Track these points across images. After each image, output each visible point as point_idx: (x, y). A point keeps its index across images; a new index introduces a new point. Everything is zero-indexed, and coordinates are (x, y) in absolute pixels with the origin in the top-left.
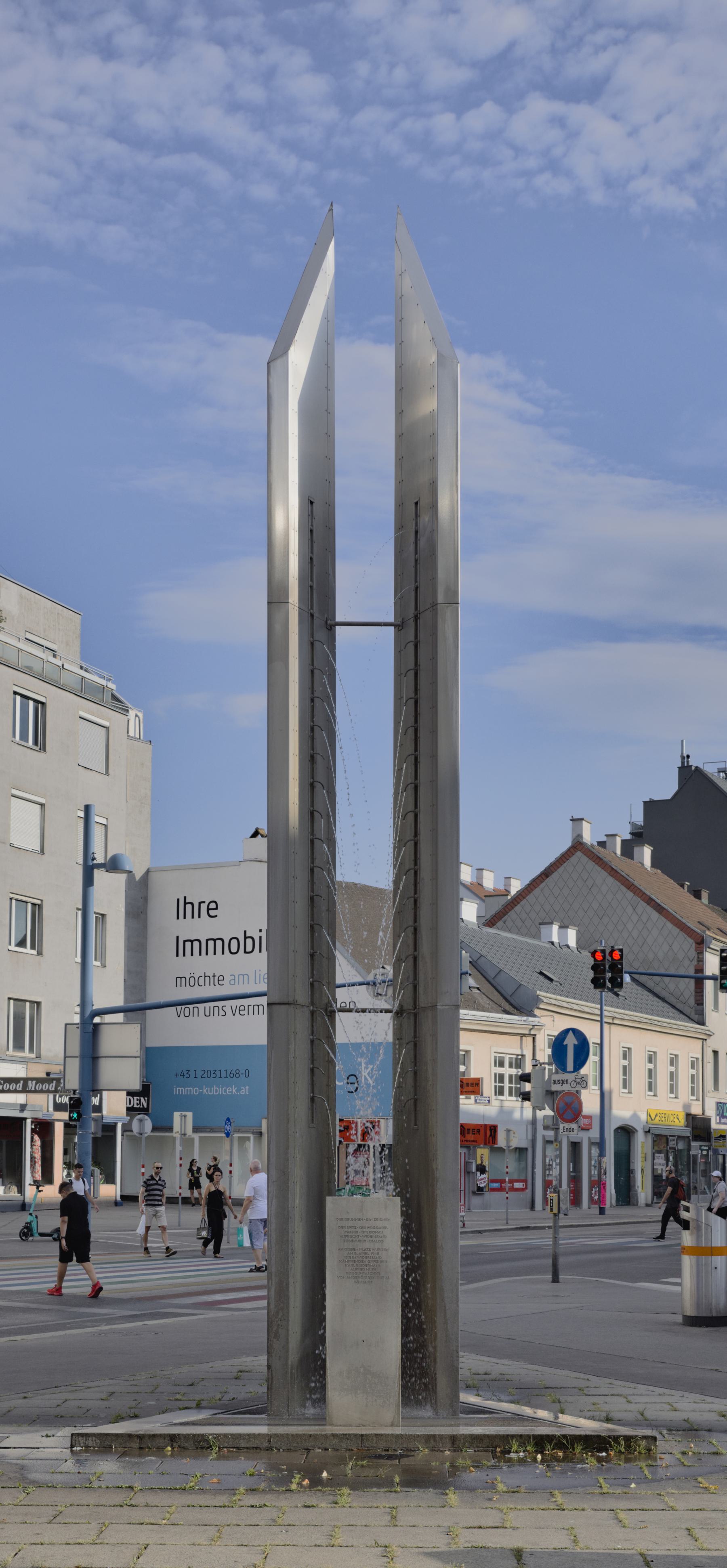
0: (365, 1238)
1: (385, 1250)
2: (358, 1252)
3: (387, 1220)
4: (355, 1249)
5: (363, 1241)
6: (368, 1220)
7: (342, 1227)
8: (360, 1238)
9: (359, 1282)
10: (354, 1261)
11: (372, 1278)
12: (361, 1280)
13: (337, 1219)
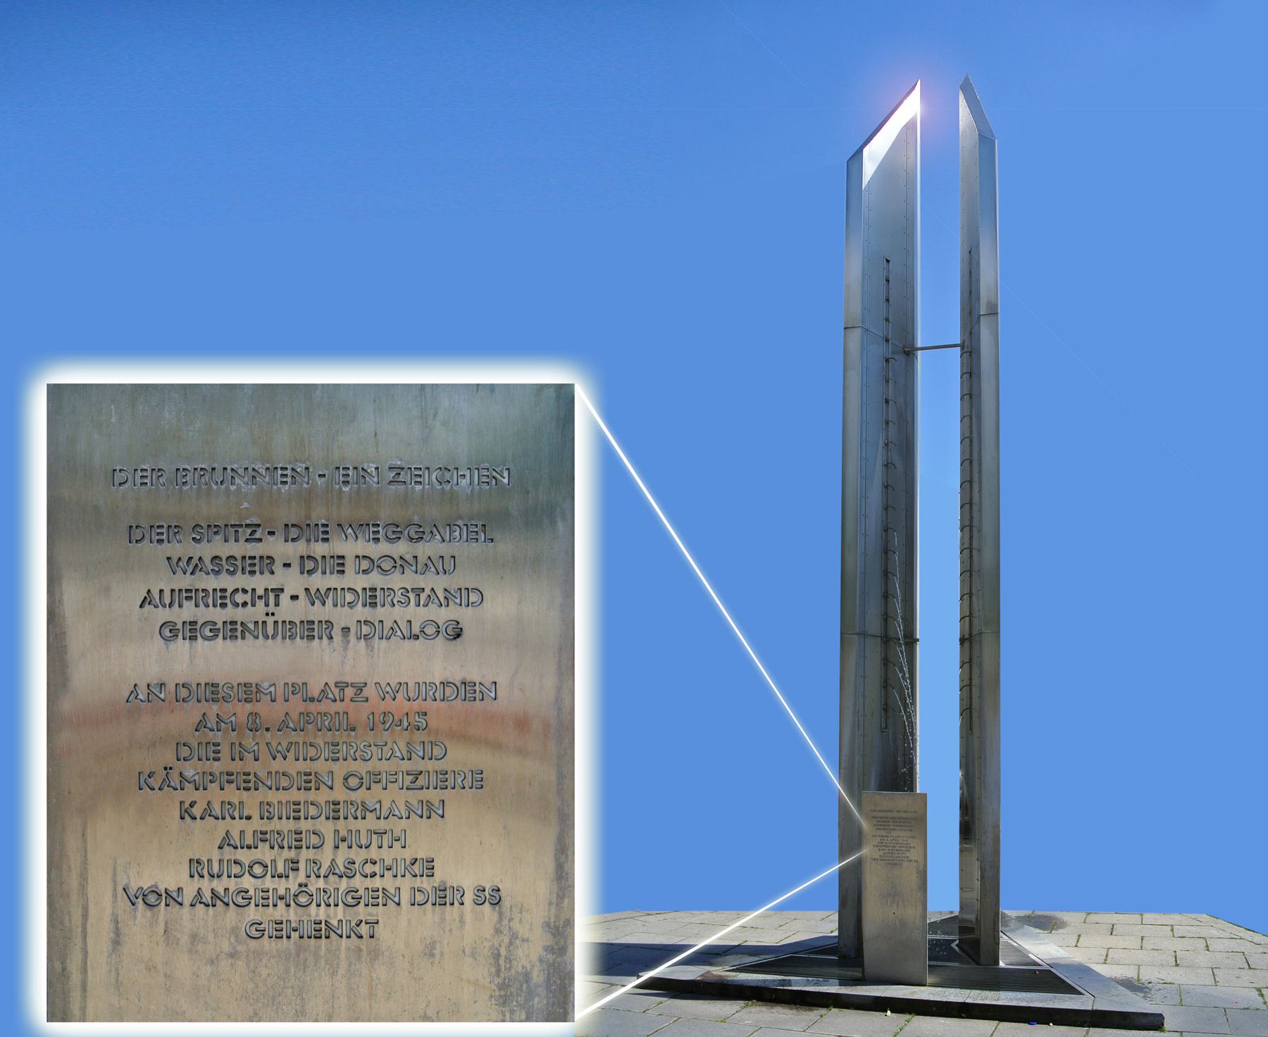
5: (310, 630)
8: (288, 610)
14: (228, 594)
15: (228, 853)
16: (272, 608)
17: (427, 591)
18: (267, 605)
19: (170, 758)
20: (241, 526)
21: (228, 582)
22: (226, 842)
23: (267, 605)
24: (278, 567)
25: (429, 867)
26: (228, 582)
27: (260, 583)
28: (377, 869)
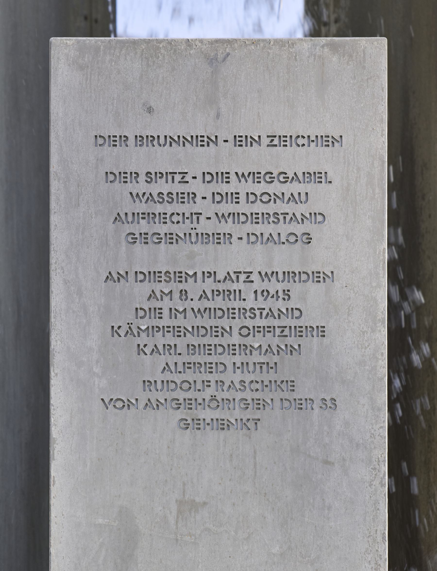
0: (227, 227)
1: (319, 277)
2: (194, 288)
3: (328, 141)
4: (181, 277)
5: (220, 238)
6: (240, 141)
7: (125, 177)
8: (205, 226)
9: (198, 424)
10: (178, 331)
11: (260, 404)
12: (207, 414)
13: (100, 140)
14: (262, 175)
15: (168, 376)
16: (195, 225)
17: (291, 215)
18: (192, 223)
19: (131, 317)
20: (176, 173)
21: (169, 209)
22: (166, 368)
23: (192, 223)
24: (198, 199)
25: (292, 385)
26: (169, 209)
27: (186, 208)
28: (259, 386)
